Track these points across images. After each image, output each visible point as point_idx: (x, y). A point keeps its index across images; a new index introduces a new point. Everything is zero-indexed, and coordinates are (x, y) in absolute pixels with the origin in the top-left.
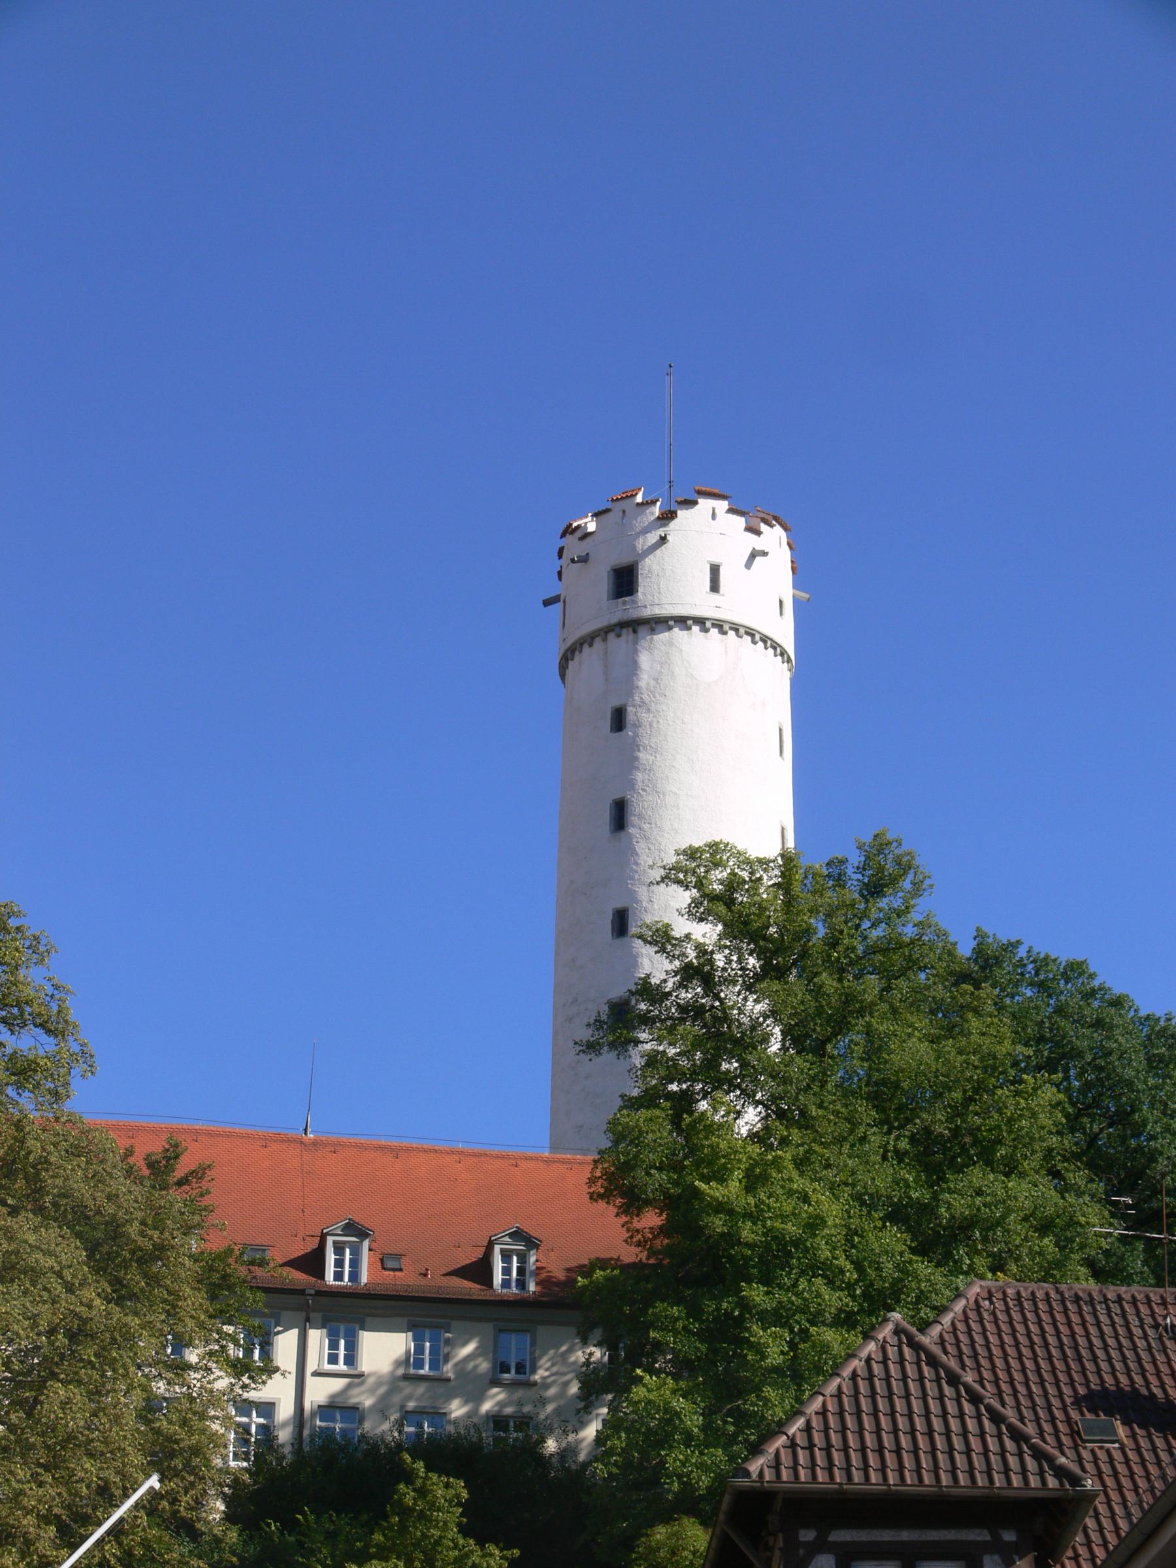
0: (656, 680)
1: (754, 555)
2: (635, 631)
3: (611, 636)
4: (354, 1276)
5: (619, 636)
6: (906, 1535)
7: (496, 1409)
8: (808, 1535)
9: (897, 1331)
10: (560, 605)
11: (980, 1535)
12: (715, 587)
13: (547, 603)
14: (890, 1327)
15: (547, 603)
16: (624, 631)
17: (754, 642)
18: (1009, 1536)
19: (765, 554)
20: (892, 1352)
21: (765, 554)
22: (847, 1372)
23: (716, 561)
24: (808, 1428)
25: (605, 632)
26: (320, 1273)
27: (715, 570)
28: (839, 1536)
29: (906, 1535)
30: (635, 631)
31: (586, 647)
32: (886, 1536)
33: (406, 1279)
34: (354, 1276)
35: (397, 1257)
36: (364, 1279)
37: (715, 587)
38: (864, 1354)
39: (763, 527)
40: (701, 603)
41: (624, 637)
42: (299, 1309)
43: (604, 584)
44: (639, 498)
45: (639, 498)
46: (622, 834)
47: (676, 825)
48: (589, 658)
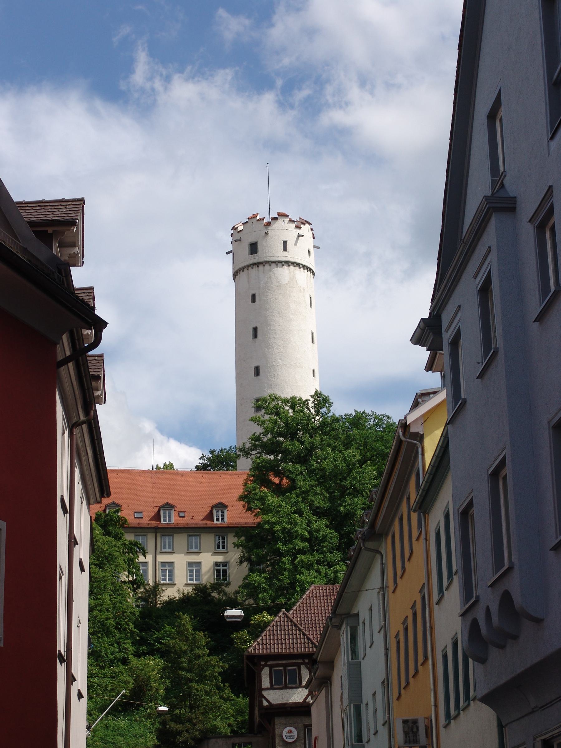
0: (266, 284)
1: (299, 236)
2: (258, 267)
3: (250, 268)
4: (170, 520)
5: (252, 268)
6: (284, 662)
7: (357, 51)
8: (263, 663)
9: (284, 614)
10: (231, 254)
11: (300, 661)
12: (285, 249)
13: (228, 253)
14: (282, 613)
15: (228, 253)
16: (254, 266)
17: (300, 268)
18: (307, 661)
19: (302, 236)
20: (282, 619)
21: (302, 236)
22: (271, 625)
23: (285, 239)
24: (262, 640)
25: (248, 266)
26: (160, 521)
27: (285, 243)
28: (269, 663)
29: (284, 662)
30: (258, 267)
31: (241, 271)
32: (280, 662)
33: (186, 521)
34: (170, 520)
35: (184, 512)
36: (173, 521)
37: (285, 249)
38: (276, 620)
39: (302, 226)
40: (281, 256)
41: (254, 269)
42: (153, 533)
43: (247, 249)
44: (258, 218)
45: (258, 218)
46: (257, 339)
47: (275, 336)
48: (243, 275)
